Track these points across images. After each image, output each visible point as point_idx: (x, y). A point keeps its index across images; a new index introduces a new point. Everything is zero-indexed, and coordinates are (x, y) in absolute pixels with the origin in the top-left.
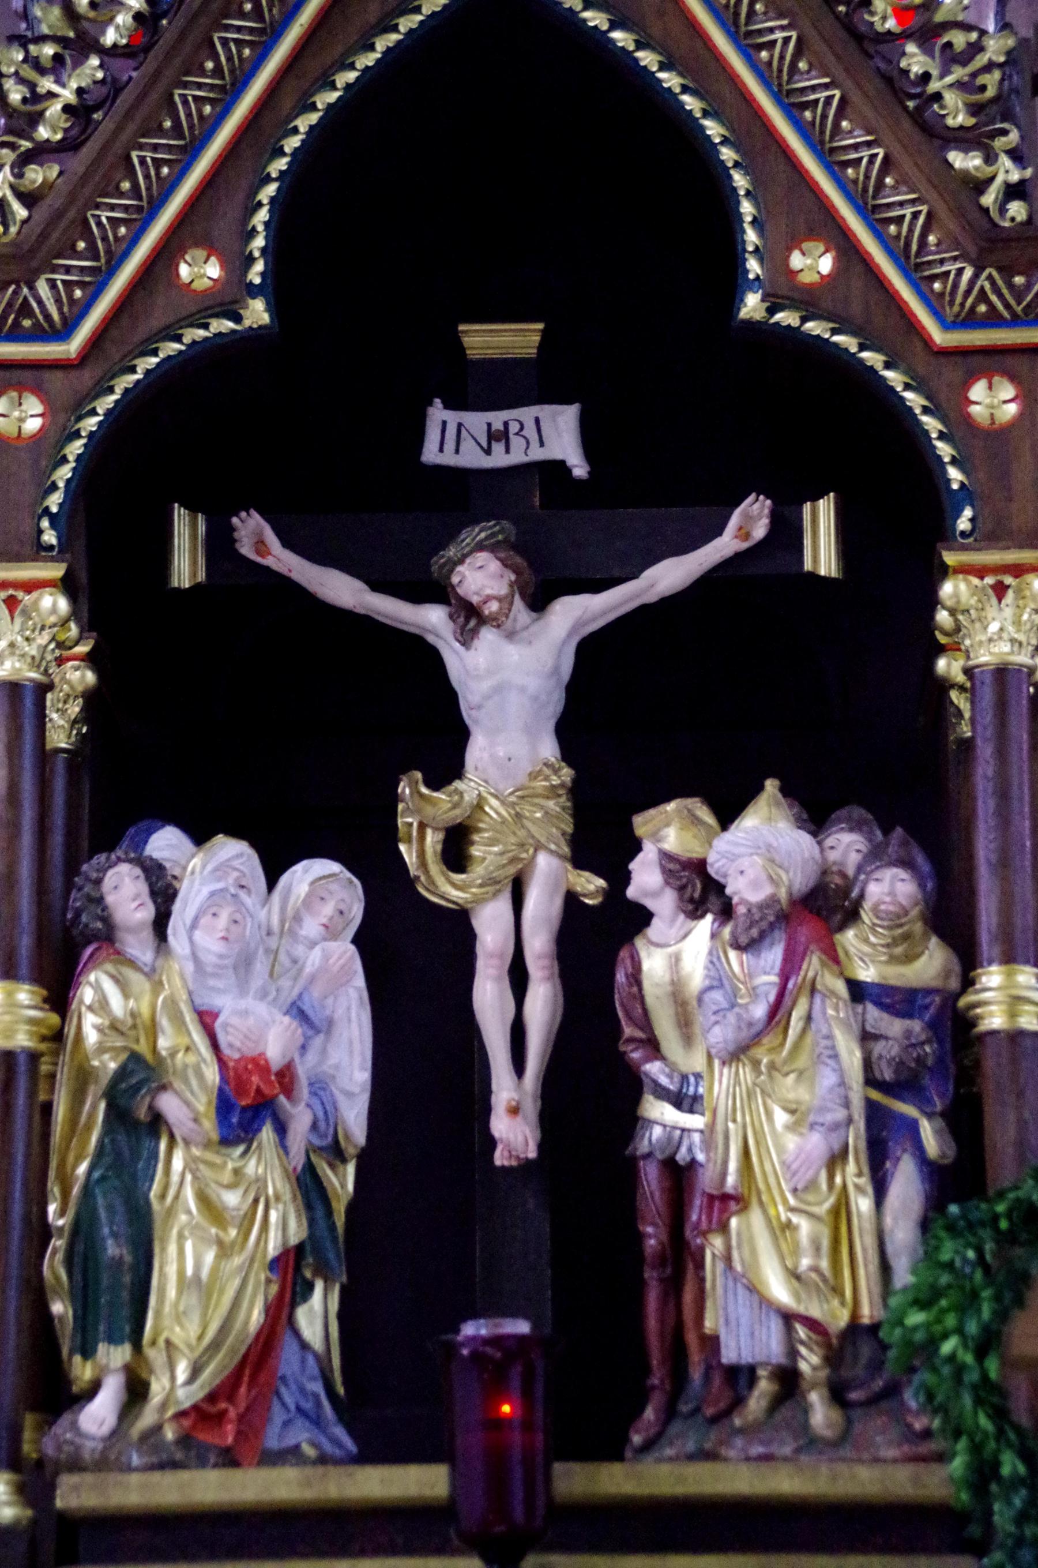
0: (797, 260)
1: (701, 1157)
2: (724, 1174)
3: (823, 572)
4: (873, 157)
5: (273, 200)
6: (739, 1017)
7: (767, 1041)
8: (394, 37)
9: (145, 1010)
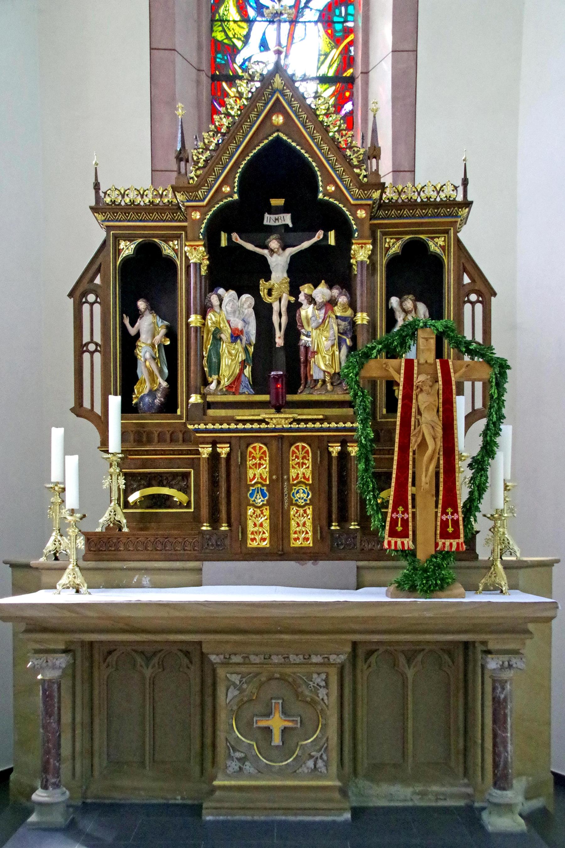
0: (328, 188)
7: (322, 325)
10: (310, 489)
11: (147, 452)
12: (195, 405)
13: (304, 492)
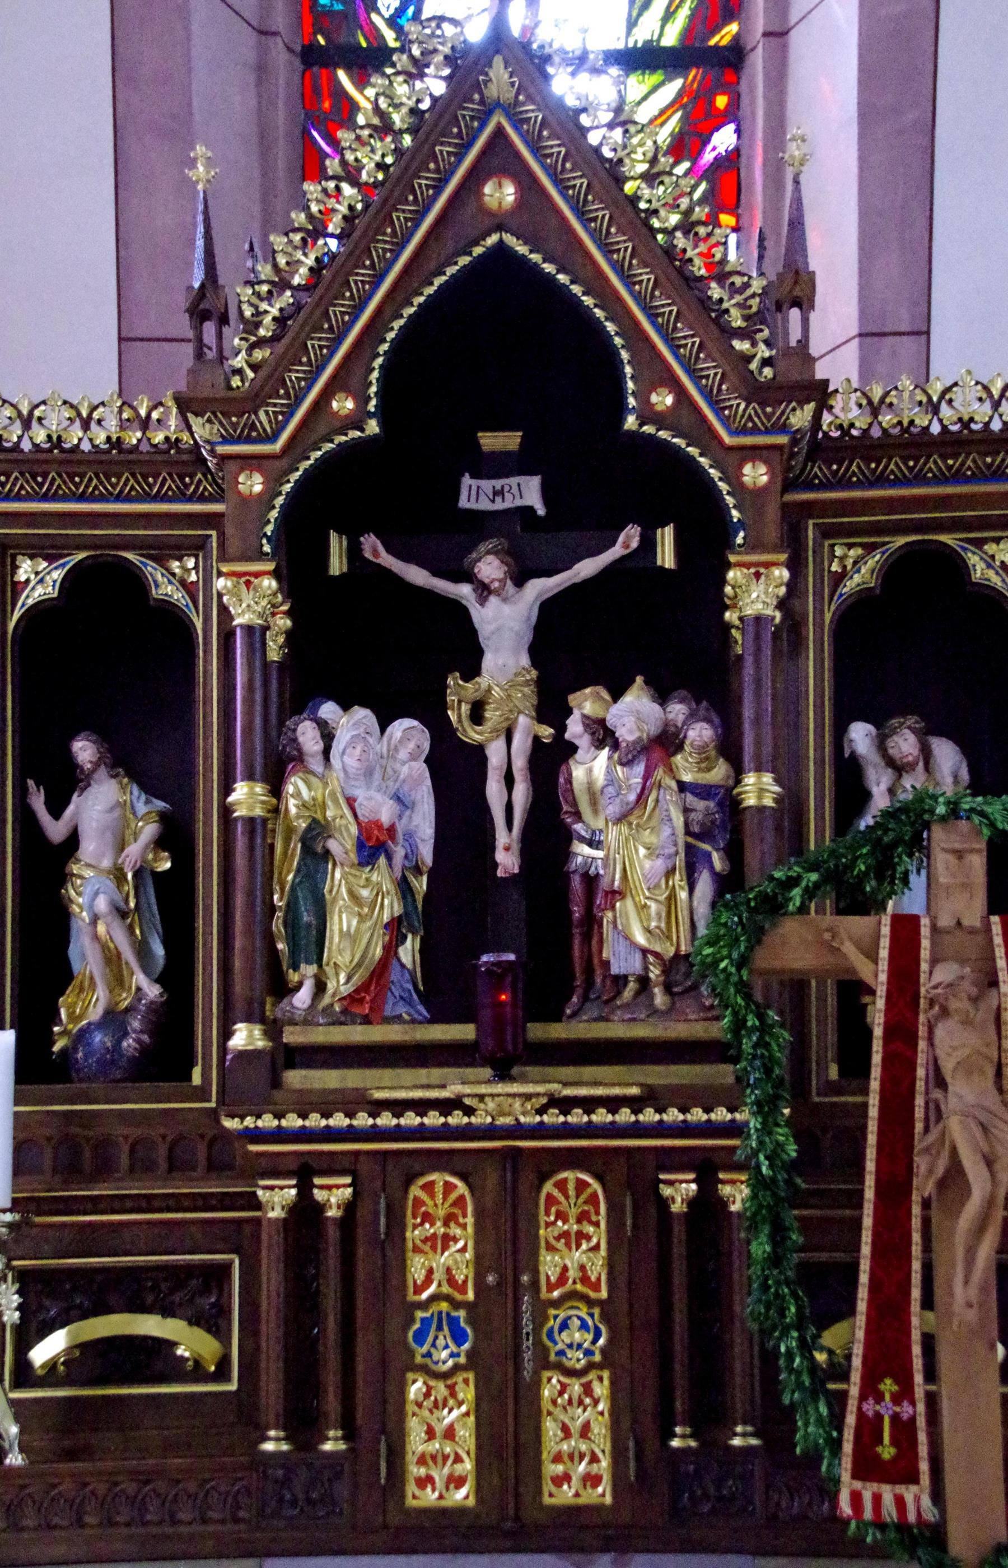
0: (654, 398)
1: (602, 872)
2: (613, 881)
3: (667, 566)
4: (694, 343)
5: (381, 366)
6: (622, 801)
8: (444, 278)
9: (319, 797)
10: (605, 1317)
11: (95, 1204)
12: (243, 1055)
13: (584, 1326)
